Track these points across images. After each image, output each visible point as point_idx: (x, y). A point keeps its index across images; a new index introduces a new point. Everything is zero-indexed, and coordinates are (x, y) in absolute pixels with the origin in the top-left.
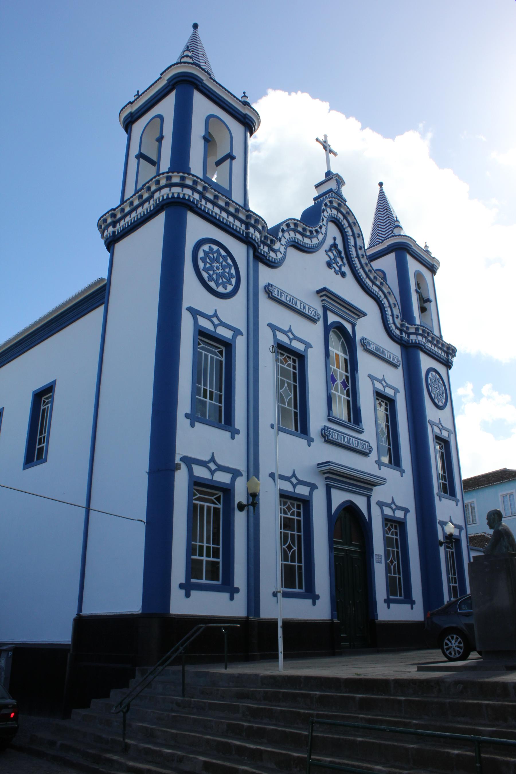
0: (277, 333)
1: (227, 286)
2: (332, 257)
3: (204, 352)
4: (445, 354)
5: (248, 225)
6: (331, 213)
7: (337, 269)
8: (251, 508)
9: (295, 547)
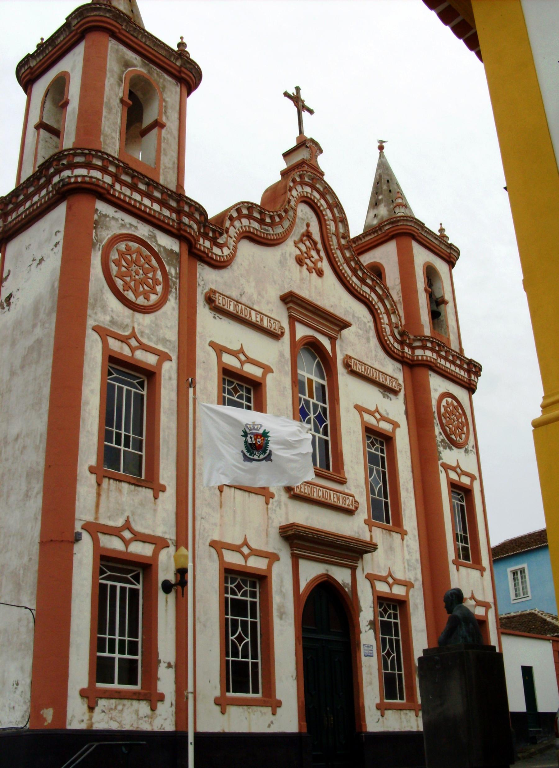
0: (364, 414)
1: (149, 296)
2: (304, 249)
3: (117, 384)
4: (466, 373)
5: (179, 212)
6: (303, 192)
7: (311, 265)
8: (180, 588)
9: (248, 637)
